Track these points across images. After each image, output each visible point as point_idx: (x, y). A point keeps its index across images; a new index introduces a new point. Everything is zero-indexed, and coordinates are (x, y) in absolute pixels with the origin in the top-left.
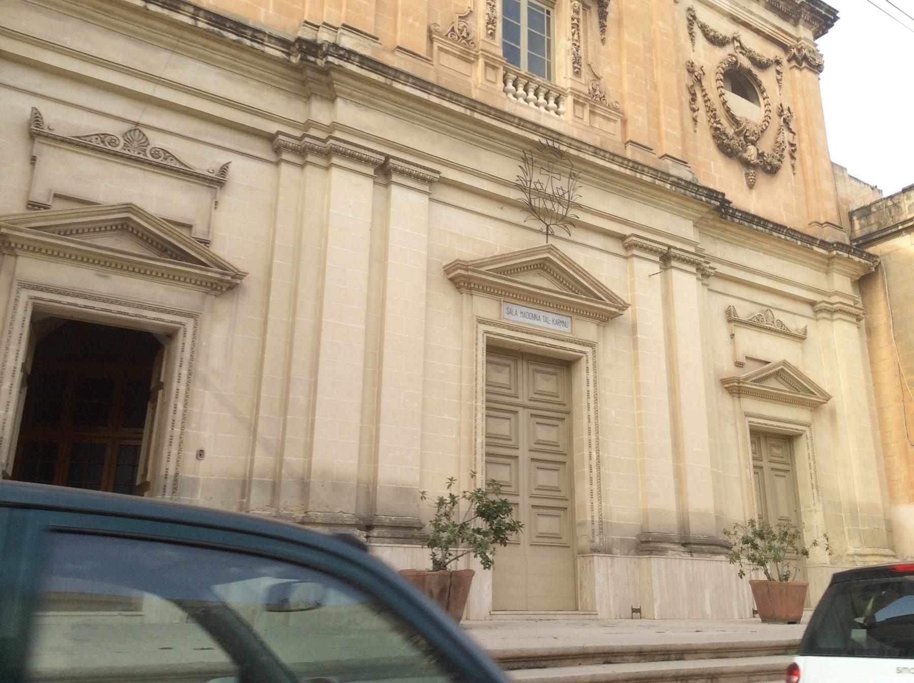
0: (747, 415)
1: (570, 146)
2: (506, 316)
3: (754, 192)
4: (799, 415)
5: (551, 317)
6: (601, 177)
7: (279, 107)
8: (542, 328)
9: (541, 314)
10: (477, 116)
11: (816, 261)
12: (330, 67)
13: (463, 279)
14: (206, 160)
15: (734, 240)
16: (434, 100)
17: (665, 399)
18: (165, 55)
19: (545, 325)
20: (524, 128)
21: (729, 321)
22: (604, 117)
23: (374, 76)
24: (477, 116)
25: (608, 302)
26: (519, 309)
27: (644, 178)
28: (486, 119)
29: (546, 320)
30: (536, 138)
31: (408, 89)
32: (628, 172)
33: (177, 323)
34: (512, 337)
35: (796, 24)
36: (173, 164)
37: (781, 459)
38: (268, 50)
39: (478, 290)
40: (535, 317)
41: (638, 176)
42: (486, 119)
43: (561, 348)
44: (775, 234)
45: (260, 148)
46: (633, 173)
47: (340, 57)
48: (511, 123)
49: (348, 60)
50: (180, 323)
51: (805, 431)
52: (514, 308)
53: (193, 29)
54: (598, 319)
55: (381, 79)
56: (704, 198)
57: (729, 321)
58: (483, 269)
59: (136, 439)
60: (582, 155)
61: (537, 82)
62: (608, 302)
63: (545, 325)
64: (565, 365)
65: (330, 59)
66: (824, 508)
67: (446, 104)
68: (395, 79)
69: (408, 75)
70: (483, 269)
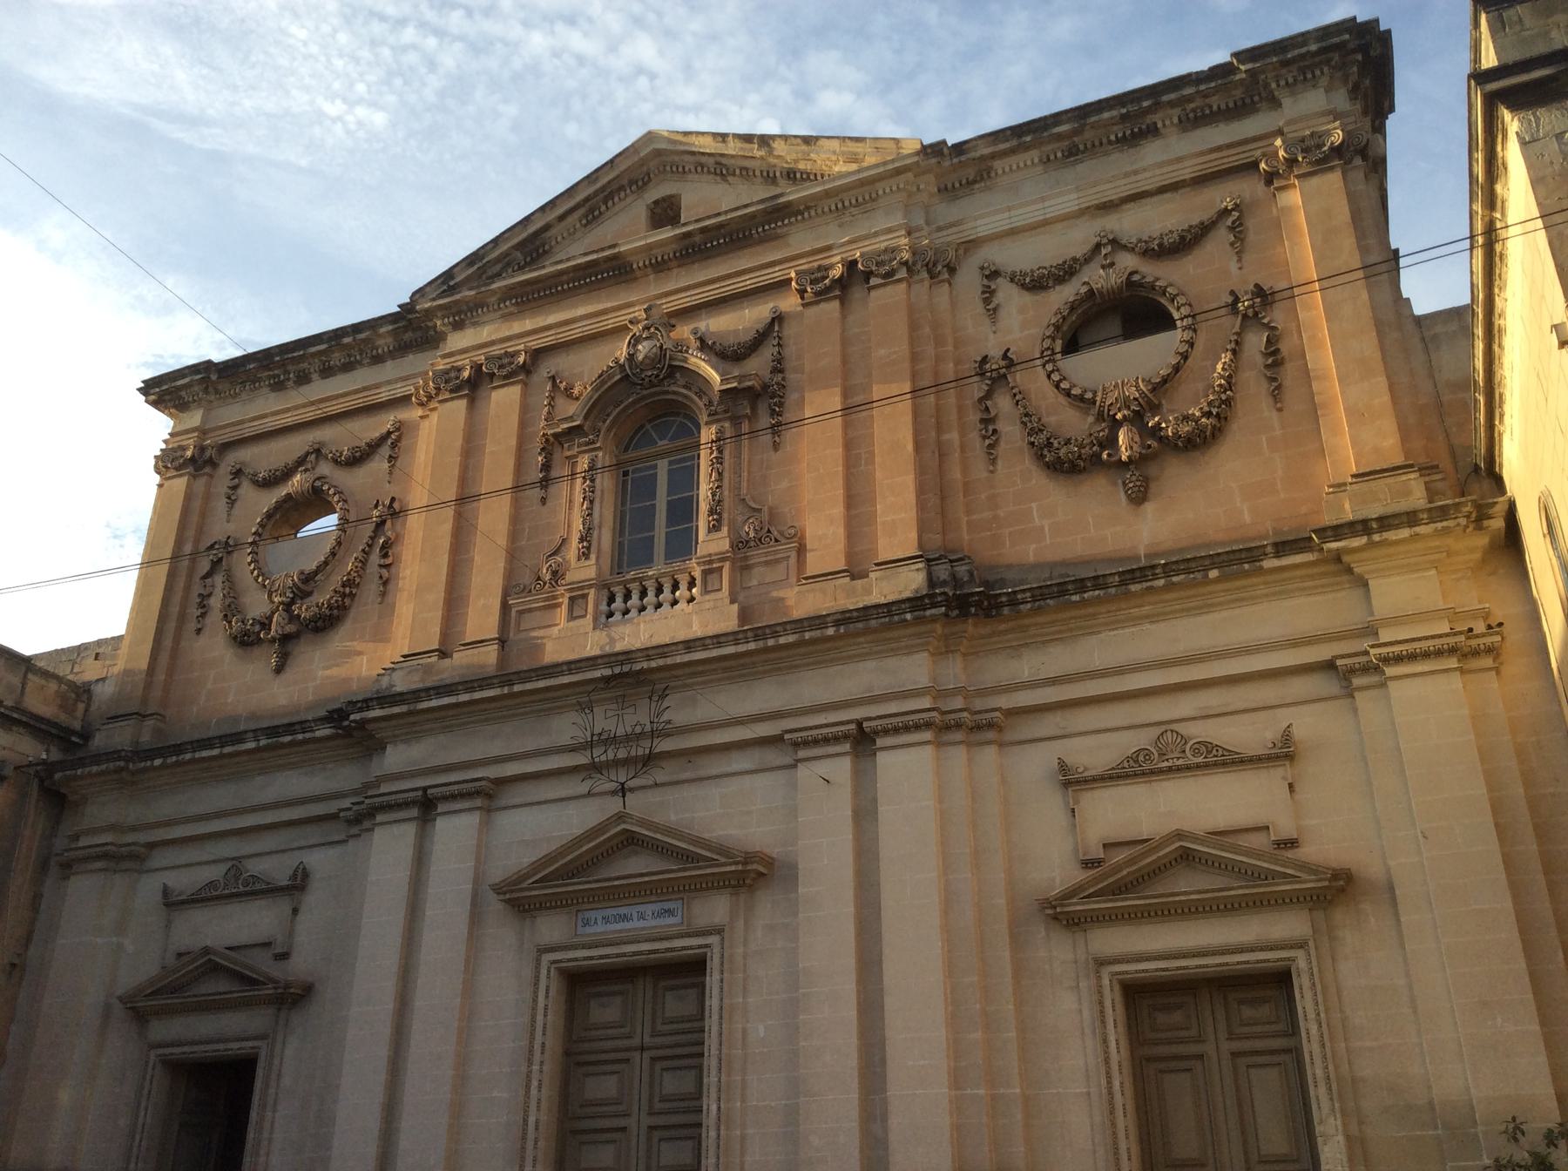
0: (1101, 963)
1: (649, 658)
2: (580, 930)
3: (1149, 507)
4: (1287, 925)
5: (649, 909)
6: (725, 670)
7: (336, 778)
8: (638, 930)
9: (634, 910)
10: (517, 688)
11: (1312, 577)
12: (362, 724)
13: (524, 897)
14: (277, 869)
15: (1060, 632)
16: (464, 697)
17: (848, 987)
18: (259, 780)
19: (642, 924)
20: (579, 670)
21: (1067, 784)
22: (767, 563)
23: (396, 710)
24: (517, 688)
25: (723, 860)
26: (599, 915)
27: (782, 640)
28: (529, 686)
29: (642, 917)
30: (597, 674)
31: (434, 703)
32: (752, 646)
33: (700, 947)
34: (591, 958)
35: (1275, 103)
36: (258, 887)
37: (1274, 1028)
38: (318, 734)
39: (541, 908)
40: (625, 918)
41: (771, 642)
42: (529, 686)
43: (667, 950)
44: (1133, 588)
45: (336, 831)
46: (761, 644)
47: (361, 710)
48: (562, 674)
49: (368, 708)
50: (707, 946)
51: (1293, 960)
52: (592, 915)
53: (258, 750)
54: (730, 886)
55: (404, 708)
56: (908, 616)
57: (1067, 784)
58: (524, 885)
59: (686, 1111)
60: (669, 661)
61: (634, 580)
62: (723, 860)
63: (642, 924)
64: (692, 969)
65: (352, 717)
66: (1344, 1125)
67: (477, 695)
68: (418, 700)
69: (427, 690)
70: (524, 885)
